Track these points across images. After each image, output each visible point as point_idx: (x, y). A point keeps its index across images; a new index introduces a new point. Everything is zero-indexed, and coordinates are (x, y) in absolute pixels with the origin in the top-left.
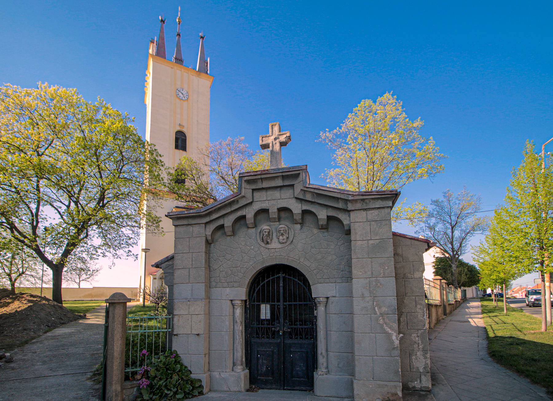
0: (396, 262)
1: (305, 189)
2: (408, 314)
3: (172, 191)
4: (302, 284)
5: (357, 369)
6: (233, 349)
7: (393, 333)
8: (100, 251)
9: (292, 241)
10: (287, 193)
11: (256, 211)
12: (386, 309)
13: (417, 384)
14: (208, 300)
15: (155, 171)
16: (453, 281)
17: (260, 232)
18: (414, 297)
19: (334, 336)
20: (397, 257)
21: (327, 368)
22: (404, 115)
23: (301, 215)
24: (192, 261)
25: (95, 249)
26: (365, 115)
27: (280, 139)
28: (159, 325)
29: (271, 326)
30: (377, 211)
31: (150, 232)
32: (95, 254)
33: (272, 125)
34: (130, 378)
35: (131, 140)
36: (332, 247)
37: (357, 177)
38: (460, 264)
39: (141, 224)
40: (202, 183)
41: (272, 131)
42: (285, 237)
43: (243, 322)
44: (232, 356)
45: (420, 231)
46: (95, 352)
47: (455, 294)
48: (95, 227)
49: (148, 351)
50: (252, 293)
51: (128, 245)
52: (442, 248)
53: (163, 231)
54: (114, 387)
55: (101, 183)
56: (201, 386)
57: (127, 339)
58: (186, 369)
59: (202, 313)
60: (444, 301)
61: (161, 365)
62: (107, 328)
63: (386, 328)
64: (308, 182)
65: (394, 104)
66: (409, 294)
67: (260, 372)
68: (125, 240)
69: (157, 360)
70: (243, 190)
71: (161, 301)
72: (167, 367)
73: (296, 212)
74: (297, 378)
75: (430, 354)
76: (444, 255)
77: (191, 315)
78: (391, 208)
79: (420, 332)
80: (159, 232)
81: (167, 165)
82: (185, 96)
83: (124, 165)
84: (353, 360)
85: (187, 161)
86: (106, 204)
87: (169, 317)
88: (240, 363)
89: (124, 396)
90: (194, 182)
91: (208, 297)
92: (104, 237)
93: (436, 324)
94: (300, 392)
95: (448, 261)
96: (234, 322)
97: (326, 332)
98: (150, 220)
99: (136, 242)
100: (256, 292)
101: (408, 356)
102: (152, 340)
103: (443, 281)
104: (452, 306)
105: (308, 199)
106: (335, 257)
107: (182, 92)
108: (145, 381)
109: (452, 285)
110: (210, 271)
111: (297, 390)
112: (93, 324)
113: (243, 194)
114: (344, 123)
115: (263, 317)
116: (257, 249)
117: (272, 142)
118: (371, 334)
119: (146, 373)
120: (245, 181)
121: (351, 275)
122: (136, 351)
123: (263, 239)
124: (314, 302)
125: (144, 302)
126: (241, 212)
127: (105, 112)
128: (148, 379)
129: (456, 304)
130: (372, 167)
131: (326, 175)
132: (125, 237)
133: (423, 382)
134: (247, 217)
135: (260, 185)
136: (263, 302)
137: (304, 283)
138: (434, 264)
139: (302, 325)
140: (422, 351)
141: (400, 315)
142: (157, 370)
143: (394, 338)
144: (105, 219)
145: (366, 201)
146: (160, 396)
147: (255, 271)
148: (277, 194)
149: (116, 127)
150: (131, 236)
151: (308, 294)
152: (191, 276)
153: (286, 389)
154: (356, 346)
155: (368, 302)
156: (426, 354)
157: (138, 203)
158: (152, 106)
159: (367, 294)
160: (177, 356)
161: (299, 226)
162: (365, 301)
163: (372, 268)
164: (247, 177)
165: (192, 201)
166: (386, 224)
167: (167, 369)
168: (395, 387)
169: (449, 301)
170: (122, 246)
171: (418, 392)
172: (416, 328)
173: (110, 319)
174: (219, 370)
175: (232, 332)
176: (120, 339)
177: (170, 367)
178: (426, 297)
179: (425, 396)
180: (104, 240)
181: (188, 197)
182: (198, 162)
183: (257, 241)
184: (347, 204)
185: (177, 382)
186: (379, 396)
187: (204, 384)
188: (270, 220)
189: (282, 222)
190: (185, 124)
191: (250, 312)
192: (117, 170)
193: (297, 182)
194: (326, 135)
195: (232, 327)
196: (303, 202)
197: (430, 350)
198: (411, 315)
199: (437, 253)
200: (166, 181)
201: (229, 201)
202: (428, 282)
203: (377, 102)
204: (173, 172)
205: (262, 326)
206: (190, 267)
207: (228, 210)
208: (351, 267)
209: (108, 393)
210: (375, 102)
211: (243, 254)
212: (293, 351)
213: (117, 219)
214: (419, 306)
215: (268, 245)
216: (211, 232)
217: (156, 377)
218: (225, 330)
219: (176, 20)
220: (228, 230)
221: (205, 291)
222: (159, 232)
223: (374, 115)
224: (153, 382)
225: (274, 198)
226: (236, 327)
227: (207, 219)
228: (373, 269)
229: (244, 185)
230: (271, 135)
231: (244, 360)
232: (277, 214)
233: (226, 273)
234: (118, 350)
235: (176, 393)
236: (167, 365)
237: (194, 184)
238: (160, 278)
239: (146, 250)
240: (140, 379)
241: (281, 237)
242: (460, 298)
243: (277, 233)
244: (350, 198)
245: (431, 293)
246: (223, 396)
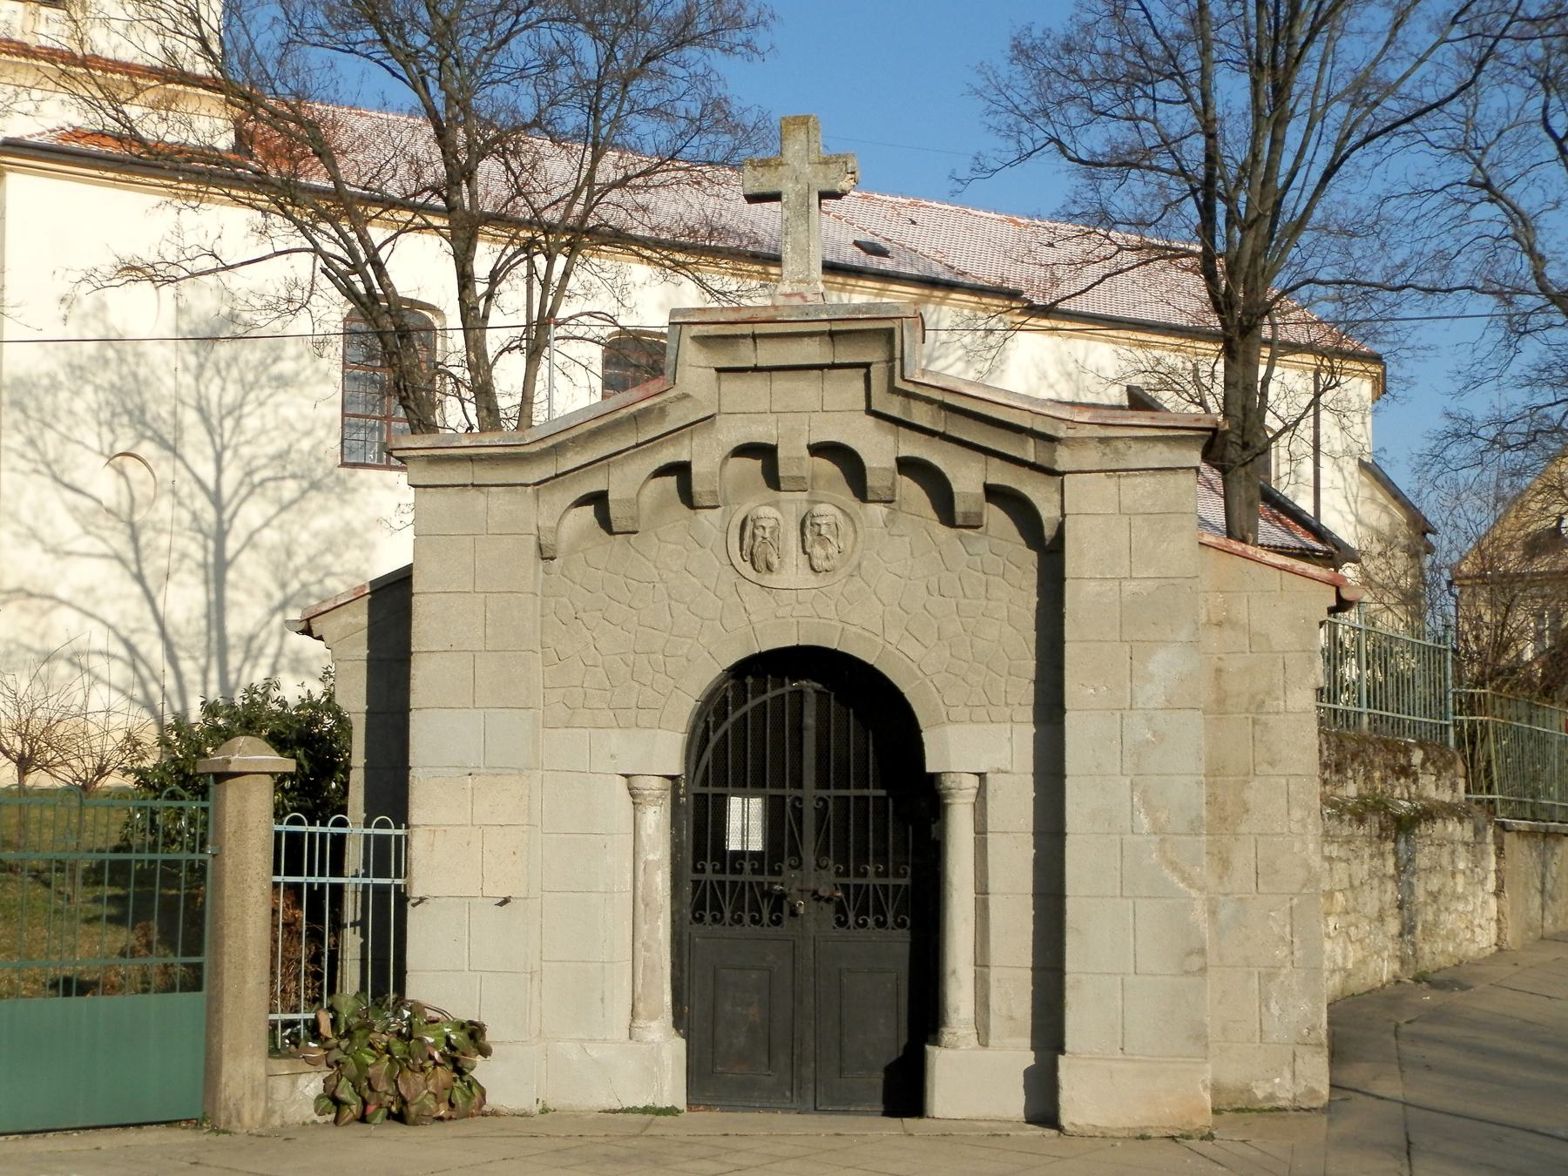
29: (766, 878)
30: (1152, 480)
115: (734, 845)
120: (694, 338)
126: (672, 449)
135: (746, 355)
139: (885, 874)
148: (804, 390)
201: (633, 409)
206: (479, 646)
218: (601, 889)
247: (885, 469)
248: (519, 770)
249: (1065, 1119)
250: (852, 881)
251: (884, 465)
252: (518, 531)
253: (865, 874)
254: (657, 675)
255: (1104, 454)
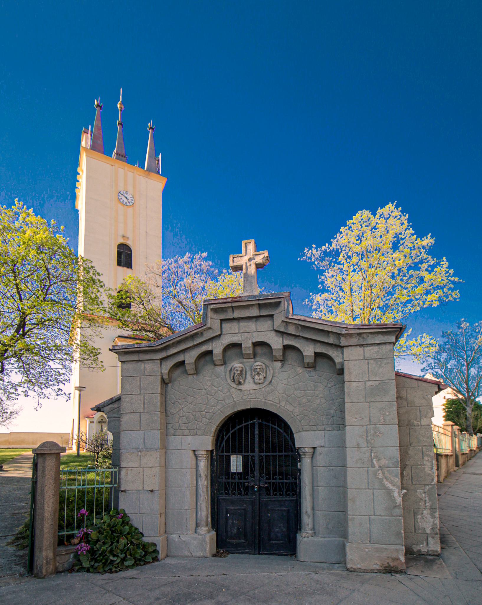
0: (399, 407)
1: (288, 320)
2: (413, 467)
3: (113, 318)
4: (282, 431)
5: (351, 530)
6: (197, 508)
7: (395, 488)
8: (20, 389)
9: (271, 381)
10: (265, 325)
11: (225, 345)
12: (387, 462)
13: (423, 548)
14: (164, 451)
15: (92, 293)
16: (467, 426)
17: (230, 371)
18: (421, 448)
19: (322, 492)
20: (401, 401)
21: (313, 529)
22: (411, 231)
23: (281, 351)
24: (144, 404)
25: (15, 387)
26: (362, 229)
27: (256, 260)
28: (98, 478)
29: (243, 481)
30: (377, 347)
31: (86, 366)
32: (13, 393)
33: (246, 243)
34: (65, 543)
35: (60, 254)
36: (321, 389)
37: (351, 304)
38: (476, 407)
39: (75, 357)
40: (152, 309)
41: (246, 251)
42: (261, 377)
43: (209, 476)
44: (194, 516)
45: (428, 368)
46: (17, 511)
47: (469, 442)
48: (13, 360)
49: (87, 510)
50: (219, 441)
51: (58, 382)
52: (454, 388)
53: (103, 366)
54: (44, 554)
55: (21, 306)
56: (156, 551)
57: (62, 497)
58: (136, 531)
59: (157, 465)
60: (455, 450)
61: (105, 527)
62: (34, 482)
63: (386, 483)
64: (291, 312)
65: (399, 217)
66: (414, 444)
67: (229, 534)
68: (54, 376)
69: (99, 521)
70: (209, 320)
71: (101, 450)
72: (112, 528)
73: (275, 348)
74: (276, 540)
75: (439, 512)
76: (456, 396)
77: (143, 467)
78: (394, 344)
79: (427, 487)
80: (98, 366)
81: (107, 286)
82: (130, 201)
83: (51, 285)
84: (346, 520)
85: (134, 282)
86: (28, 331)
87: (115, 470)
88: (205, 524)
89: (58, 564)
90: (143, 307)
91: (165, 447)
92: (26, 372)
93: (446, 477)
94: (280, 556)
95: (461, 403)
96: (198, 476)
97: (313, 488)
98: (85, 353)
99: (68, 379)
100: (225, 440)
101: (413, 515)
102: (93, 497)
103: (455, 427)
104: (466, 455)
105: (290, 332)
106: (323, 401)
107: (126, 195)
108: (84, 546)
109: (466, 431)
110: (167, 416)
111: (276, 554)
112: (13, 477)
113: (209, 325)
114: (335, 238)
116: (226, 390)
117: (246, 263)
118: (367, 490)
119: (85, 536)
120: (212, 309)
121: (344, 421)
122: (72, 510)
123: (234, 379)
124: (298, 452)
125: (78, 450)
126: (206, 346)
127: (25, 219)
128: (89, 544)
129: (471, 453)
130: (369, 291)
131: (311, 301)
132: (54, 373)
133: (430, 545)
134: (214, 352)
136: (234, 452)
137: (284, 431)
138: (444, 407)
139: (282, 479)
140: (430, 509)
141: (403, 467)
142: (100, 532)
143: (396, 494)
144: (26, 350)
145: (363, 335)
146: (103, 563)
147: (224, 417)
148: (251, 326)
149: (39, 238)
150: (61, 372)
151: (290, 443)
152: (142, 422)
153: (261, 554)
154: (350, 504)
155: (365, 453)
156: (434, 512)
157: (69, 331)
158: (87, 212)
159: (363, 444)
160: (125, 516)
161: (279, 364)
162: (361, 452)
163: (370, 413)
164: (214, 305)
165: (140, 330)
166: (388, 363)
167: (113, 532)
168: (397, 551)
169: (462, 450)
170: (50, 383)
171: (424, 556)
172: (423, 483)
173: (40, 473)
174: (179, 532)
175: (194, 488)
176: (52, 496)
177: (116, 529)
178: (434, 445)
179: (433, 561)
180: (26, 375)
181: (135, 325)
182: (148, 282)
183: (226, 380)
184: (339, 339)
185: (125, 546)
186: (377, 562)
187: (159, 548)
188: (242, 356)
189: (258, 359)
190: (129, 235)
191: (216, 464)
192: (42, 291)
193: (277, 311)
194: (312, 252)
195: (195, 482)
196: (285, 336)
197: (439, 508)
198: (417, 468)
199: (448, 394)
200: (106, 305)
201: (191, 333)
202: (436, 429)
203: (377, 214)
204: (115, 294)
205: (233, 481)
206: (142, 410)
207: (190, 344)
208: (344, 412)
209: (37, 561)
210: (374, 214)
211: (208, 396)
212: (272, 510)
213: (43, 350)
214: (426, 458)
215: (240, 386)
216: (168, 370)
217: (98, 540)
218: (186, 486)
219: (117, 107)
220: (190, 368)
221: (161, 440)
222: (98, 366)
223: (373, 230)
224: (95, 547)
225: (248, 330)
226: (199, 481)
227: (163, 355)
228: (371, 415)
229: (210, 314)
230: (244, 255)
231: (210, 520)
232: (251, 349)
233: (187, 418)
234: (50, 509)
235: (124, 560)
236: (113, 527)
237: (143, 310)
238: (99, 422)
239: (80, 389)
240: (78, 544)
241: (257, 377)
242: (476, 446)
243: (252, 372)
244: (344, 332)
245: (440, 441)
246: (183, 562)
247: (279, 349)
248: (156, 449)
249: (219, 320)
250: (271, 481)
251: (279, 348)
252: (155, 374)
253: (276, 479)
254: (203, 419)
255: (359, 339)
